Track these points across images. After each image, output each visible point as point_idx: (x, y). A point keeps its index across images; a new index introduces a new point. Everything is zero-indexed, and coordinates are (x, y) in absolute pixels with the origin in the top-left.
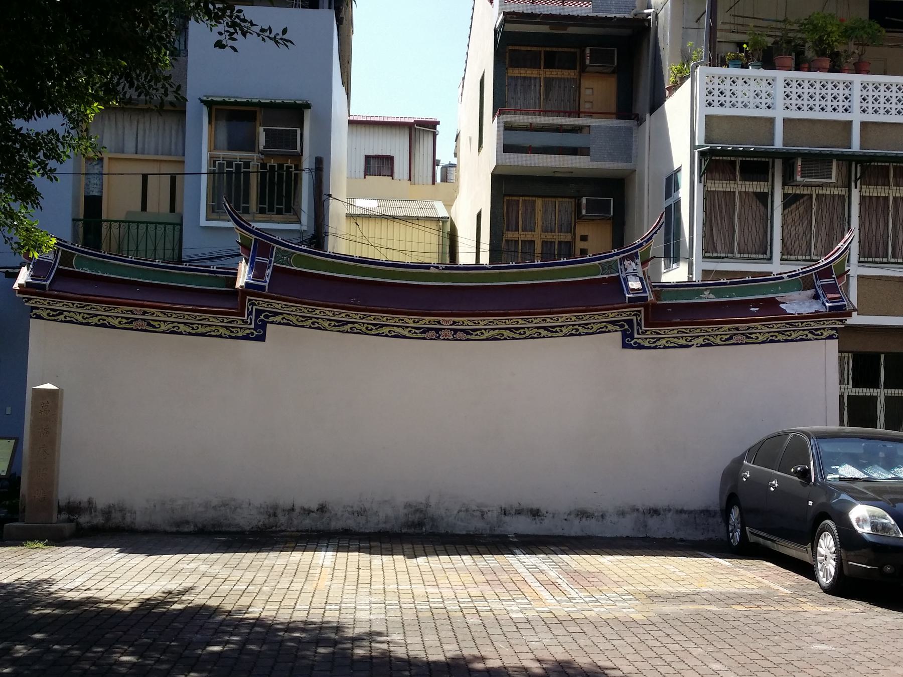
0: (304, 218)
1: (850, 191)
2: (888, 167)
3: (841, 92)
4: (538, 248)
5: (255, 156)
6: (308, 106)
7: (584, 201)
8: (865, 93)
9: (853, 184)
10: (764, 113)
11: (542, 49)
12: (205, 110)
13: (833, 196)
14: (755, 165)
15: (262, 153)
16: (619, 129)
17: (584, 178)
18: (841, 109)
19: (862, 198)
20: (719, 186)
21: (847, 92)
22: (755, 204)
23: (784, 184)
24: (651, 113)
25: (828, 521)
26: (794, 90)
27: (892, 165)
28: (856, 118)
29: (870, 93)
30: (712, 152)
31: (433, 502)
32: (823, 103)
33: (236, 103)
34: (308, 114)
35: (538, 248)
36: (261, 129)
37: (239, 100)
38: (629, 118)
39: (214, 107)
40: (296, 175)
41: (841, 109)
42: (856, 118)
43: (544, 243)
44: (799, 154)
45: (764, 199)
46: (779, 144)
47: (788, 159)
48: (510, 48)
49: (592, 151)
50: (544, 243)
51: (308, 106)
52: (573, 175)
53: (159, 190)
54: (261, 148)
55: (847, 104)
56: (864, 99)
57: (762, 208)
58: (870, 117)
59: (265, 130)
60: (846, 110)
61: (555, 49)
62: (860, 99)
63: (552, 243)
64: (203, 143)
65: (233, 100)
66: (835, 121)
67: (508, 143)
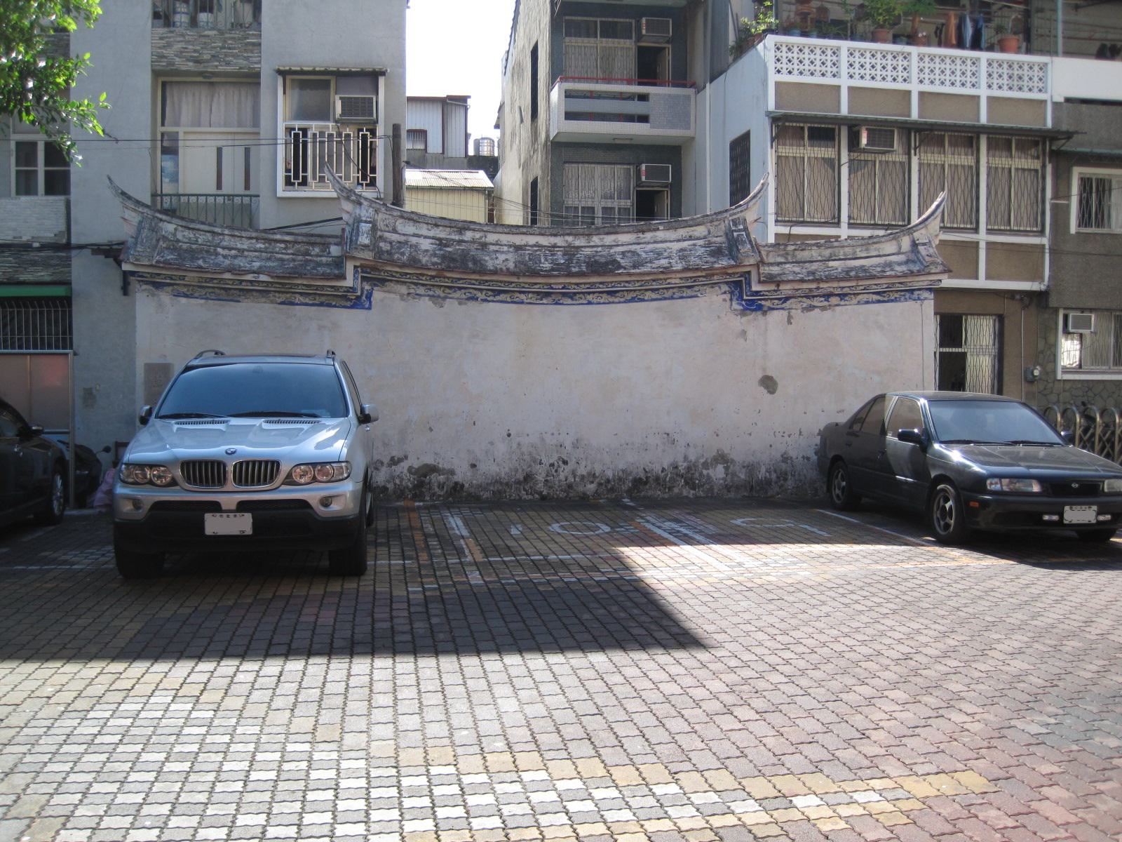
0: (380, 182)
1: (910, 159)
2: (802, 128)
3: (829, 58)
4: (599, 213)
5: (331, 124)
6: (383, 73)
7: (643, 167)
8: (852, 59)
9: (913, 152)
10: (828, 81)
11: (599, 20)
12: (280, 80)
13: (894, 163)
14: (823, 131)
15: (336, 122)
16: (677, 96)
17: (642, 146)
18: (900, 79)
19: (920, 165)
20: (790, 151)
21: (974, 68)
22: (1029, 177)
23: (850, 151)
24: (711, 81)
25: (942, 486)
26: (868, 60)
27: (806, 126)
28: (844, 83)
29: (927, 65)
30: (786, 118)
31: (541, 474)
32: (884, 73)
33: (314, 72)
34: (382, 81)
35: (599, 213)
36: (337, 97)
37: (305, 69)
38: (684, 86)
39: (289, 78)
40: (371, 142)
41: (900, 79)
42: (915, 88)
43: (605, 209)
44: (866, 121)
45: (833, 165)
46: (844, 111)
47: (853, 127)
48: (567, 18)
49: (651, 119)
50: (605, 209)
51: (383, 73)
52: (632, 142)
53: (233, 160)
54: (337, 116)
55: (905, 74)
56: (851, 65)
57: (830, 171)
58: (927, 88)
59: (341, 98)
60: (905, 80)
61: (616, 20)
62: (847, 65)
63: (612, 209)
64: (280, 110)
65: (287, 68)
66: (895, 90)
67: (569, 110)
